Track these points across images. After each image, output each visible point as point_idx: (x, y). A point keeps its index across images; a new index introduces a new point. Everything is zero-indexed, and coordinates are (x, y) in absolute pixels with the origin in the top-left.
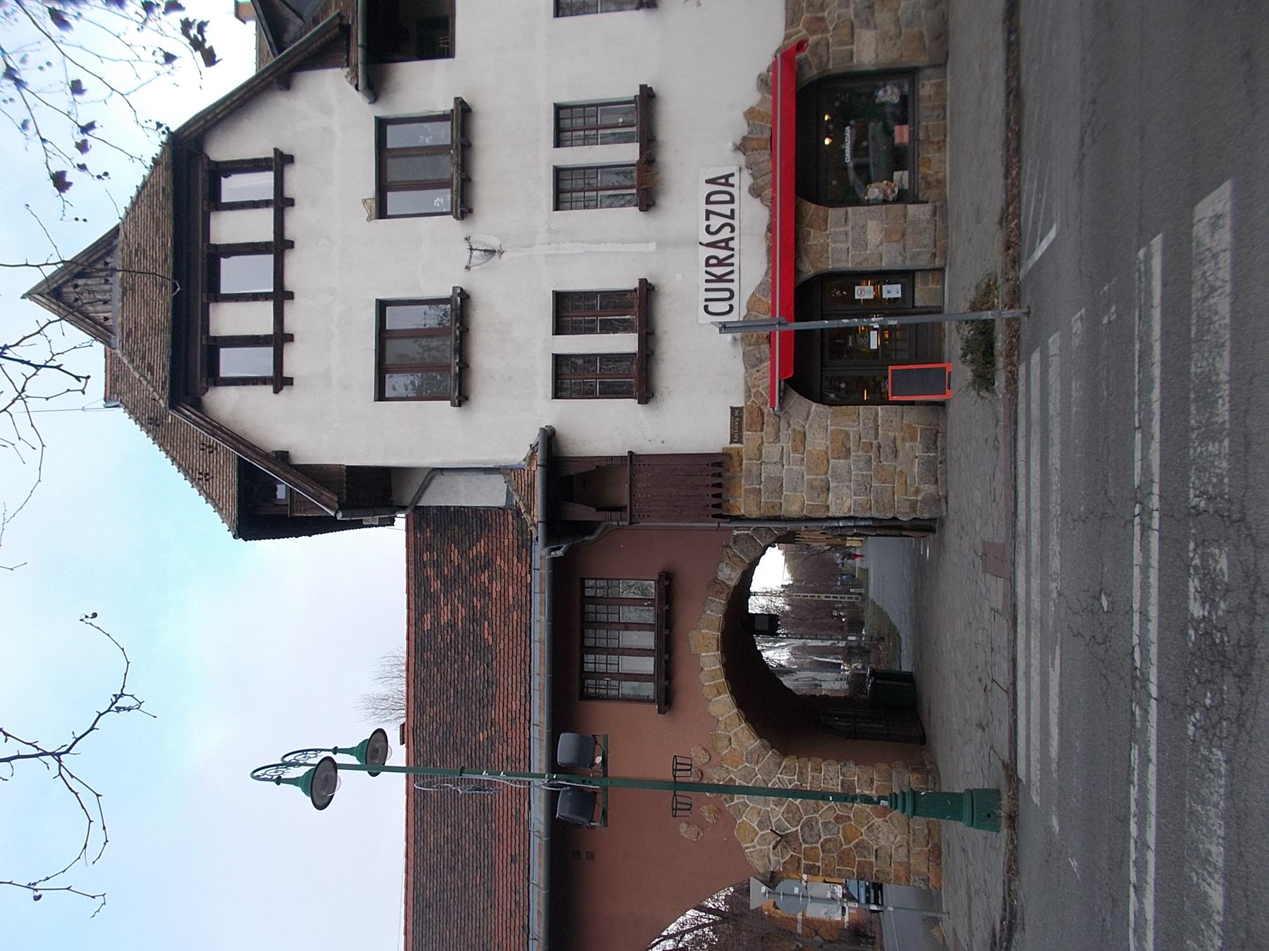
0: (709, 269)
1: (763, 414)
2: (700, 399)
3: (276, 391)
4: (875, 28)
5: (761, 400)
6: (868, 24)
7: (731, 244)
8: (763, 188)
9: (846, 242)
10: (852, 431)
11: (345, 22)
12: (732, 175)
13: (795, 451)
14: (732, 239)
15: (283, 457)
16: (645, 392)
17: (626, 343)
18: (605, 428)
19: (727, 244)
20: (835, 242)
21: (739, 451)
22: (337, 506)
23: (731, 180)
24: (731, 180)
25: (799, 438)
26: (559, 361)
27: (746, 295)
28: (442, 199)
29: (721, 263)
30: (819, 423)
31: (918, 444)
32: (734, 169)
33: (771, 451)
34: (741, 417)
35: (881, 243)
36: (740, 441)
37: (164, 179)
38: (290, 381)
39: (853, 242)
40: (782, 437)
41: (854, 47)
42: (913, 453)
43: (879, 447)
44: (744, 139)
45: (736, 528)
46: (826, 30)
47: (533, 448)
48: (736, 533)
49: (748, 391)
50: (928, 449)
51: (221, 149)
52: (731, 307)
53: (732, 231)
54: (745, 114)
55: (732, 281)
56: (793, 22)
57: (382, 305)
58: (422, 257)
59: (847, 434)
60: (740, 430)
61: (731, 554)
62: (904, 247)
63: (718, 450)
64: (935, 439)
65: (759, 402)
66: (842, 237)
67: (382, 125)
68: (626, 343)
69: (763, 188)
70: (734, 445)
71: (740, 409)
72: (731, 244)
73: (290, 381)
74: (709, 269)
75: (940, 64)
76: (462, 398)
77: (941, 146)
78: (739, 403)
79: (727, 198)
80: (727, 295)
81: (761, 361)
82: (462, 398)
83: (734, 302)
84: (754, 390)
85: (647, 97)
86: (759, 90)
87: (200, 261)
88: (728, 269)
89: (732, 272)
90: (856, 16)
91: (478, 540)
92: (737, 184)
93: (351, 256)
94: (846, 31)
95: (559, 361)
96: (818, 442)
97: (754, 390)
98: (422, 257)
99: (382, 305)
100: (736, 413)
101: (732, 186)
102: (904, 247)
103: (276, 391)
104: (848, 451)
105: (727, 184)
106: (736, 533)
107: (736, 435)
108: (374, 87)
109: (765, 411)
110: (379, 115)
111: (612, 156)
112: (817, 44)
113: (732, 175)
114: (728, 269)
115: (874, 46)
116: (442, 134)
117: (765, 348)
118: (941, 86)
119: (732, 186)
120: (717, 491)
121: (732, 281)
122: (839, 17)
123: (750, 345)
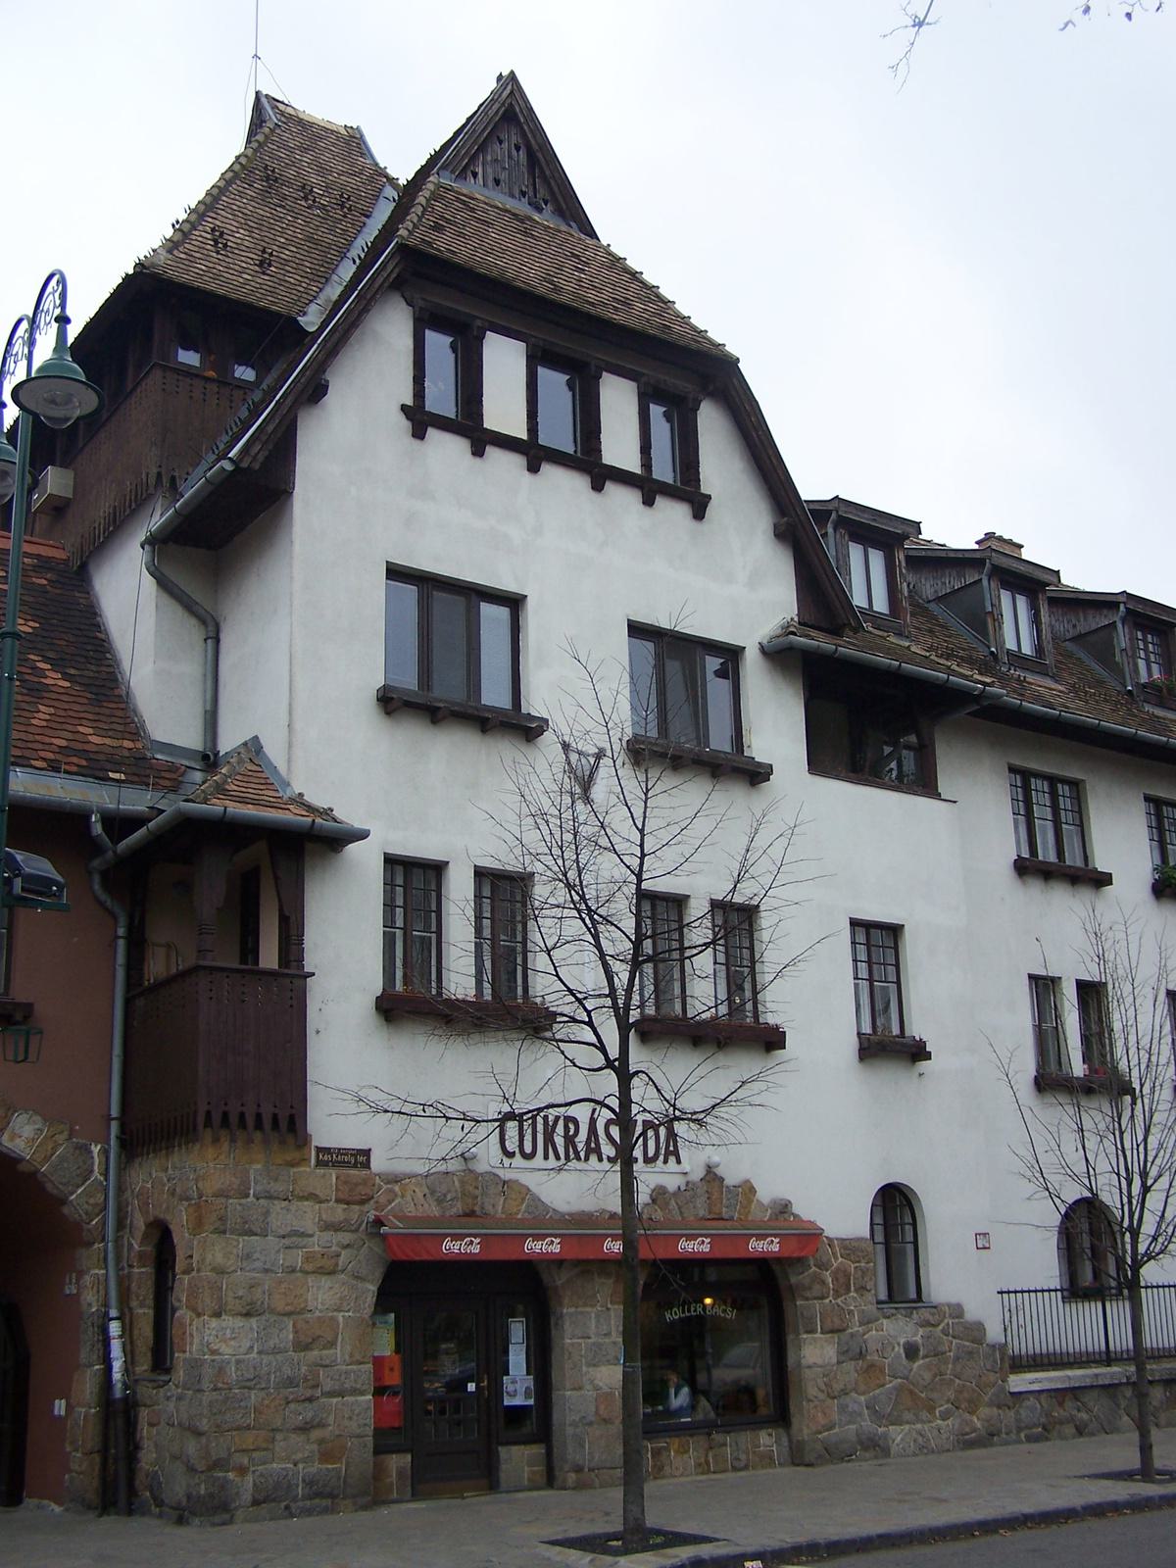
0: (561, 1122)
1: (362, 1202)
2: (376, 1092)
3: (404, 408)
4: (839, 1363)
5: (383, 1200)
6: (844, 1354)
7: (593, 1158)
8: (665, 1206)
9: (598, 1335)
10: (339, 1352)
11: (847, 631)
12: (679, 1162)
13: (308, 1258)
14: (600, 1160)
15: (315, 391)
16: (393, 1009)
17: (460, 978)
18: (344, 938)
19: (672, 1153)
20: (598, 1316)
21: (305, 1160)
22: (244, 465)
23: (672, 1159)
24: (672, 1159)
25: (328, 1263)
26: (435, 870)
27: (530, 1180)
28: (409, 681)
29: (570, 1140)
30: (342, 1298)
31: (316, 1467)
32: (686, 1166)
33: (306, 1217)
34: (355, 1166)
35: (597, 1388)
36: (319, 1163)
37: (634, 317)
38: (419, 434)
39: (599, 1346)
40: (327, 1235)
41: (818, 1335)
42: (292, 1459)
43: (310, 1400)
44: (722, 1180)
45: (105, 1152)
46: (837, 1295)
47: (327, 813)
48: (96, 1149)
49: (395, 1179)
50: (309, 1483)
51: (711, 424)
52: (510, 1155)
53: (609, 1159)
54: (747, 1182)
55: (546, 1157)
56: (846, 1248)
57: (514, 603)
58: (580, 682)
59: (332, 1344)
60: (336, 1164)
61: (60, 1138)
62: (590, 1424)
63: (311, 1127)
64: (325, 1497)
65: (381, 1197)
66: (604, 1329)
67: (731, 655)
68: (460, 978)
69: (665, 1206)
70: (313, 1153)
71: (367, 1165)
72: (593, 1158)
73: (419, 434)
74: (561, 1122)
75: (798, 1457)
76: (390, 702)
77: (703, 1468)
78: (378, 1164)
79: (651, 1153)
80: (528, 1149)
81: (439, 1201)
82: (390, 702)
83: (518, 1161)
84: (397, 1188)
85: (772, 1040)
86: (774, 1202)
87: (464, 307)
88: (561, 1151)
89: (558, 1158)
90: (852, 1335)
91: (66, 677)
92: (666, 1168)
93: (597, 575)
94: (837, 1322)
95: (435, 870)
96: (322, 1294)
97: (397, 1188)
98: (580, 682)
99: (514, 603)
100: (361, 1158)
101: (665, 1162)
102: (590, 1424)
103: (404, 408)
104: (307, 1347)
105: (668, 1153)
106: (96, 1149)
107: (332, 1158)
108: (778, 655)
109: (366, 1207)
110: (747, 652)
111: (697, 986)
112: (823, 1282)
113: (679, 1162)
114: (561, 1151)
115: (820, 1361)
116: (719, 740)
117: (458, 1208)
118: (767, 1460)
119: (665, 1162)
120: (250, 1121)
121: (546, 1157)
122: (851, 1312)
123: (462, 1182)
